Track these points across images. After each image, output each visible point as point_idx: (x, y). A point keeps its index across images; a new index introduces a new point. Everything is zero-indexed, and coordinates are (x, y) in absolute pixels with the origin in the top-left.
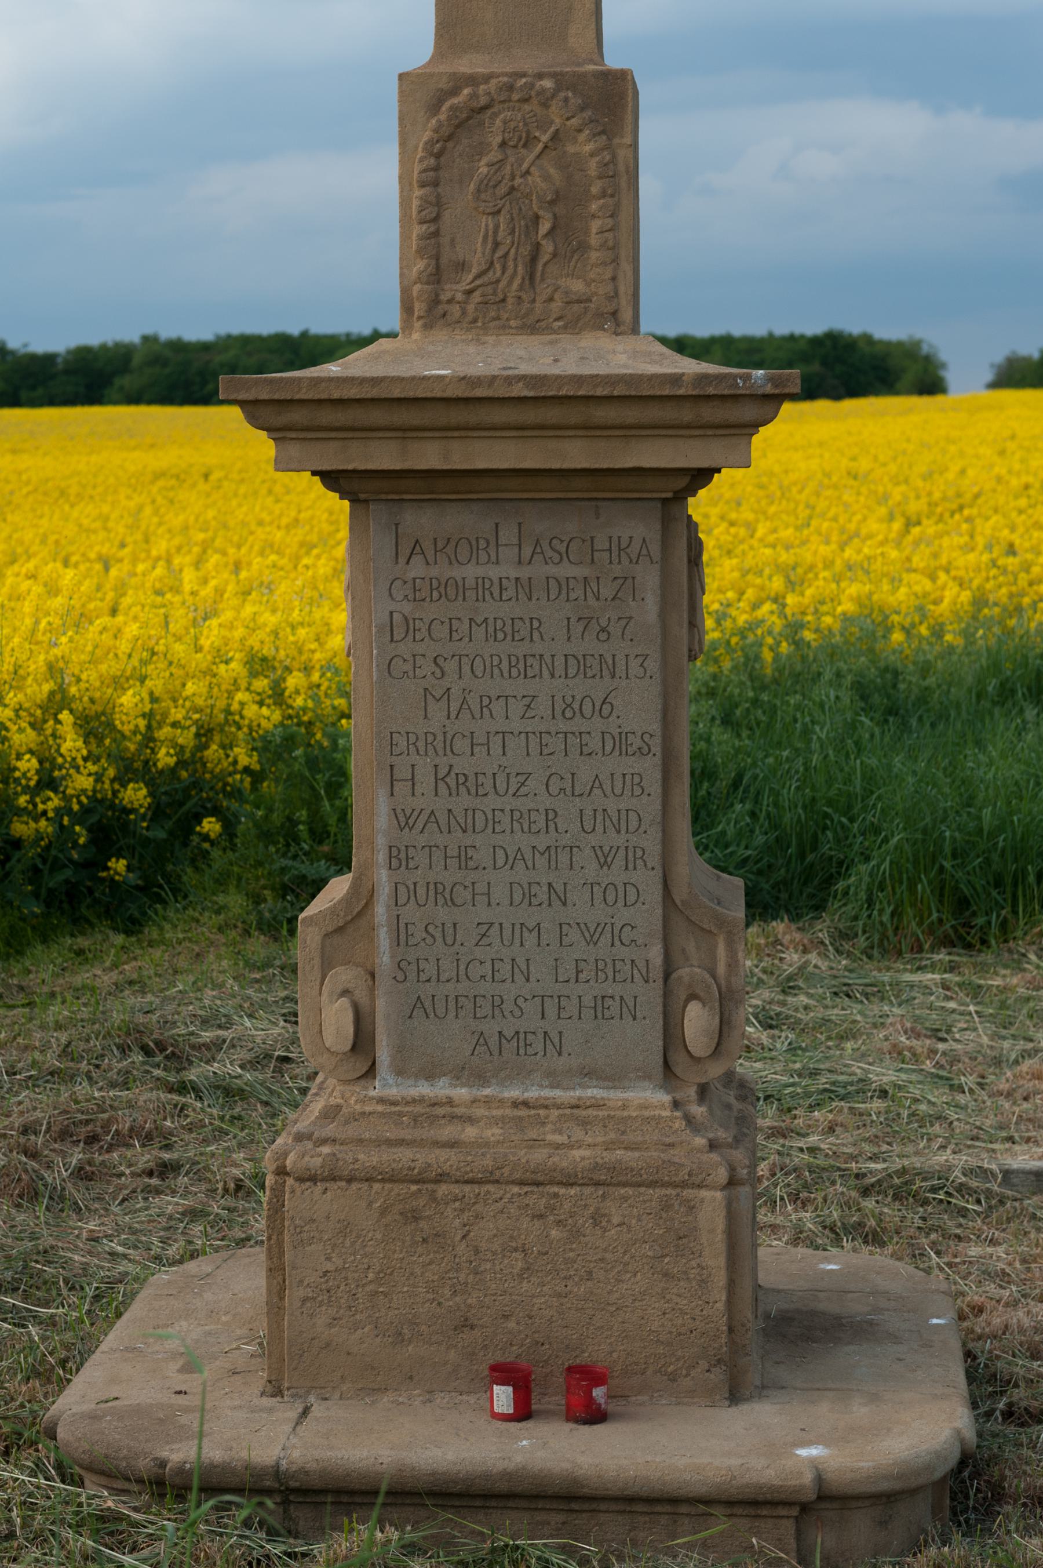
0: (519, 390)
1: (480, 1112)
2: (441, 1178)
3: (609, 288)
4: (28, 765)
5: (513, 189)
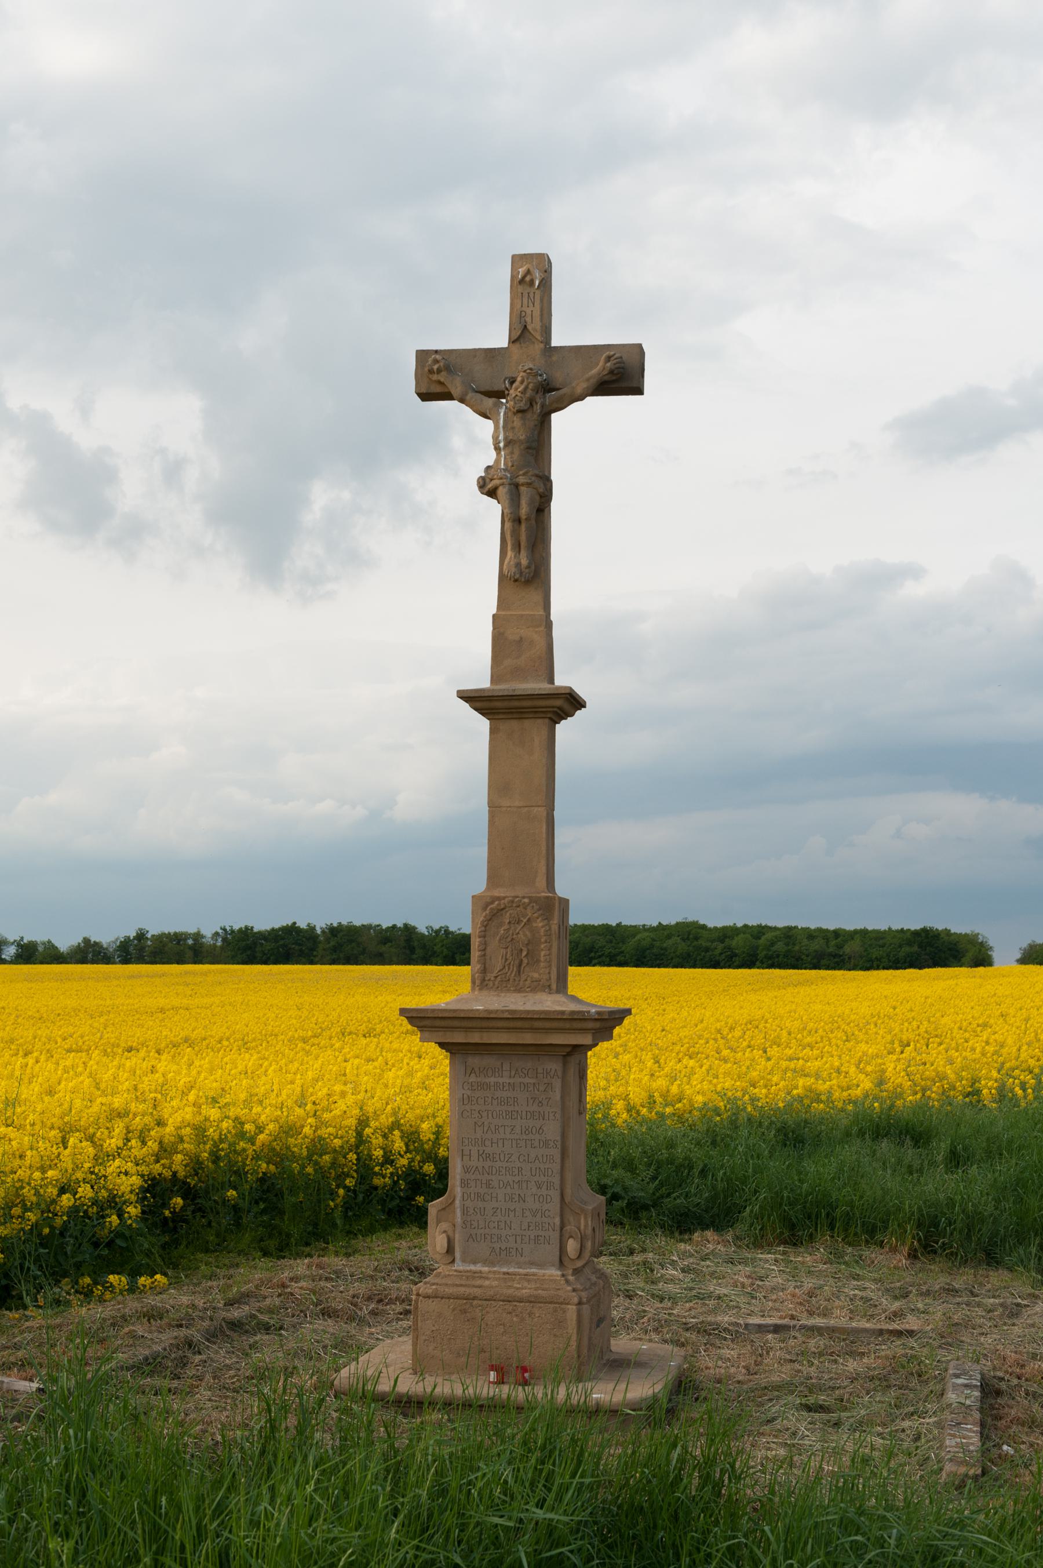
0: (506, 1015)
1: (491, 1276)
2: (474, 1298)
3: (547, 976)
4: (378, 1153)
5: (513, 939)
